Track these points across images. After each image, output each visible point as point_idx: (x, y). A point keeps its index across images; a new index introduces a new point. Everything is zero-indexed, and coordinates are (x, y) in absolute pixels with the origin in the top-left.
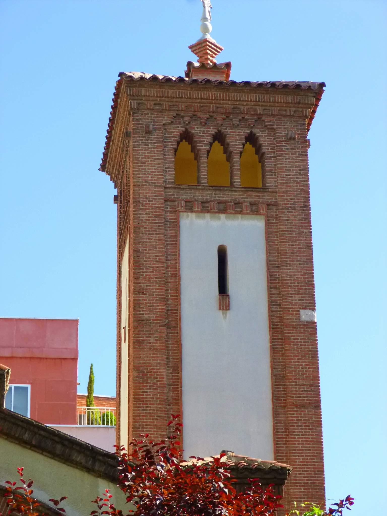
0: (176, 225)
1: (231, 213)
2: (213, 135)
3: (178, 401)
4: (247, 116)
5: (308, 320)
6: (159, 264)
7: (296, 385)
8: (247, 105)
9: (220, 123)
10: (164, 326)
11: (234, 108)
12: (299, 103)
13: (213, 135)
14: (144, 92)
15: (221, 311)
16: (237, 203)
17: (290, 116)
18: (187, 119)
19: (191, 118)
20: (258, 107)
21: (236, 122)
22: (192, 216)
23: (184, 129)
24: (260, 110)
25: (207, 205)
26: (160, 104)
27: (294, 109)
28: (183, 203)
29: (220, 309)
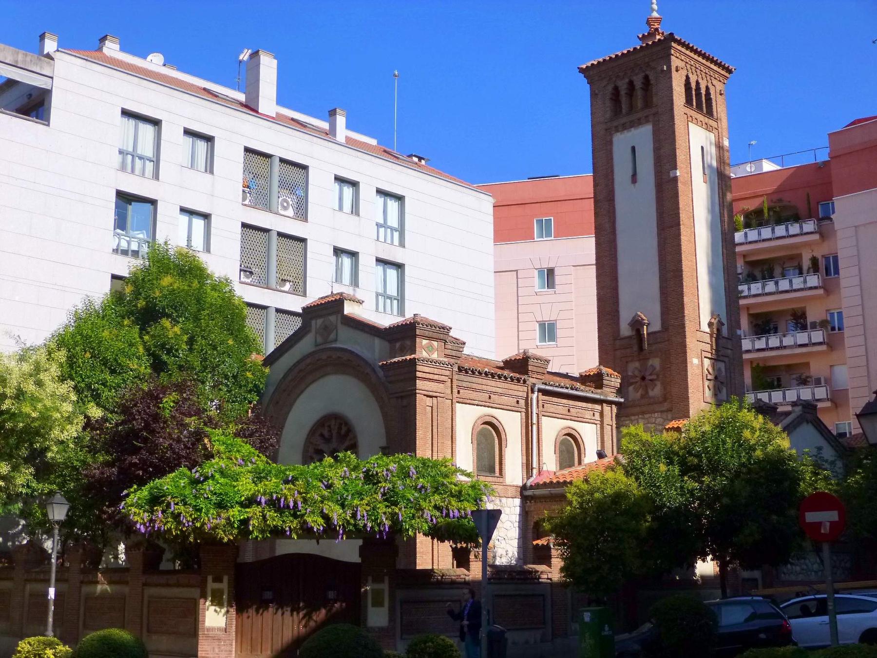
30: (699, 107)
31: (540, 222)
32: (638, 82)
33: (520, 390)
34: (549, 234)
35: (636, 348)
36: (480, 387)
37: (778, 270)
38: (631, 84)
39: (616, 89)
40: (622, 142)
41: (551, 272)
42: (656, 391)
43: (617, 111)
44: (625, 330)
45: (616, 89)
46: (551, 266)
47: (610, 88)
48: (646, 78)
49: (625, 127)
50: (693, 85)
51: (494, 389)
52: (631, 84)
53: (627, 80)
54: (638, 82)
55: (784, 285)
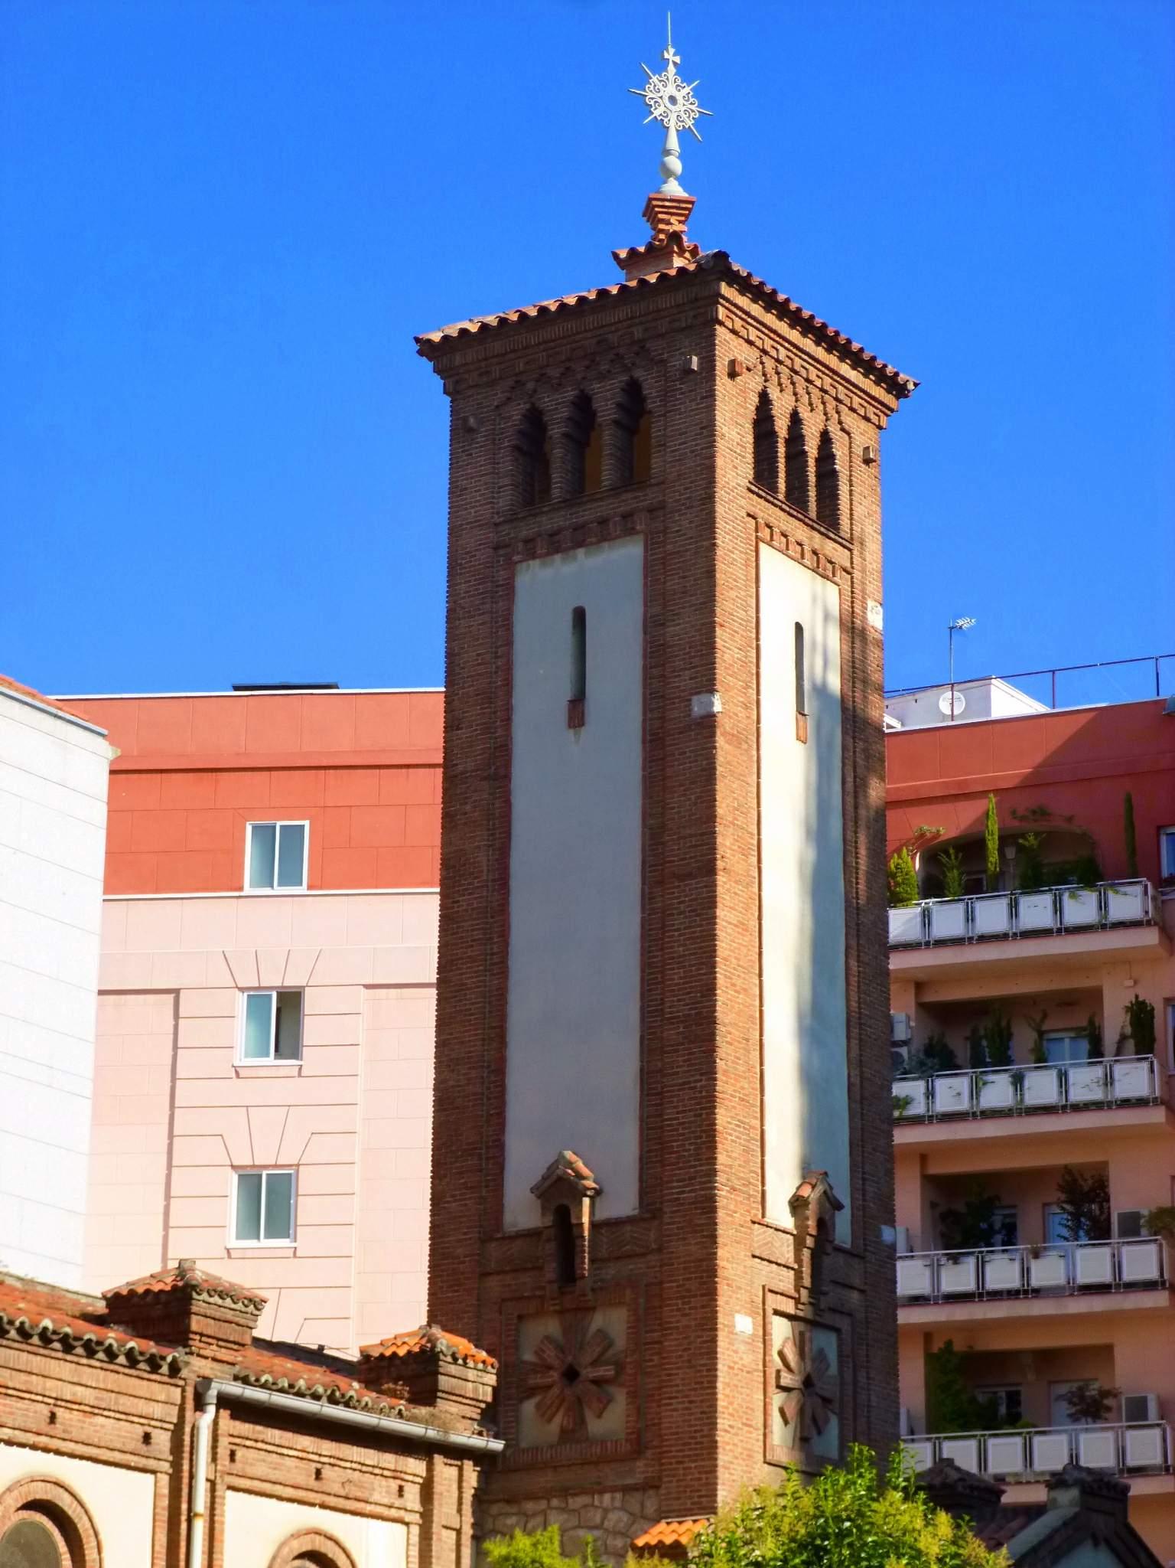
0: (509, 590)
1: (592, 544)
2: (573, 403)
3: (502, 910)
4: (621, 351)
5: (703, 712)
6: (482, 669)
7: (679, 838)
8: (617, 331)
9: (579, 377)
10: (485, 779)
11: (599, 342)
12: (696, 300)
13: (573, 403)
14: (458, 359)
15: (572, 731)
16: (603, 522)
17: (689, 327)
18: (530, 385)
19: (537, 381)
20: (634, 329)
21: (604, 367)
22: (535, 564)
23: (528, 406)
24: (638, 333)
25: (557, 538)
26: (487, 372)
27: (691, 313)
28: (520, 546)
29: (570, 727)
30: (796, 499)
31: (265, 834)
32: (607, 402)
33: (158, 1399)
34: (291, 877)
35: (551, 1271)
36: (19, 1380)
37: (1023, 1038)
38: (584, 405)
39: (535, 420)
40: (545, 589)
41: (290, 1002)
42: (611, 1421)
43: (533, 490)
44: (521, 1210)
45: (535, 420)
46: (292, 981)
47: (516, 412)
48: (634, 390)
49: (557, 544)
50: (782, 426)
51: (68, 1391)
52: (584, 405)
53: (571, 394)
54: (607, 402)
55: (1042, 1087)
